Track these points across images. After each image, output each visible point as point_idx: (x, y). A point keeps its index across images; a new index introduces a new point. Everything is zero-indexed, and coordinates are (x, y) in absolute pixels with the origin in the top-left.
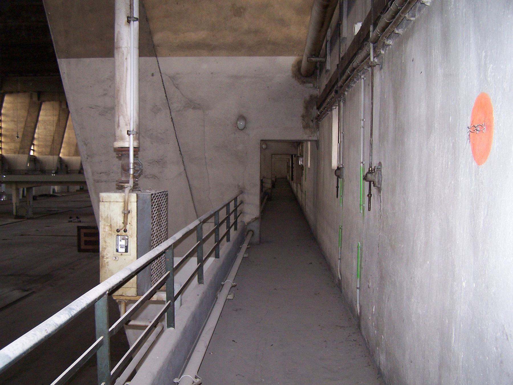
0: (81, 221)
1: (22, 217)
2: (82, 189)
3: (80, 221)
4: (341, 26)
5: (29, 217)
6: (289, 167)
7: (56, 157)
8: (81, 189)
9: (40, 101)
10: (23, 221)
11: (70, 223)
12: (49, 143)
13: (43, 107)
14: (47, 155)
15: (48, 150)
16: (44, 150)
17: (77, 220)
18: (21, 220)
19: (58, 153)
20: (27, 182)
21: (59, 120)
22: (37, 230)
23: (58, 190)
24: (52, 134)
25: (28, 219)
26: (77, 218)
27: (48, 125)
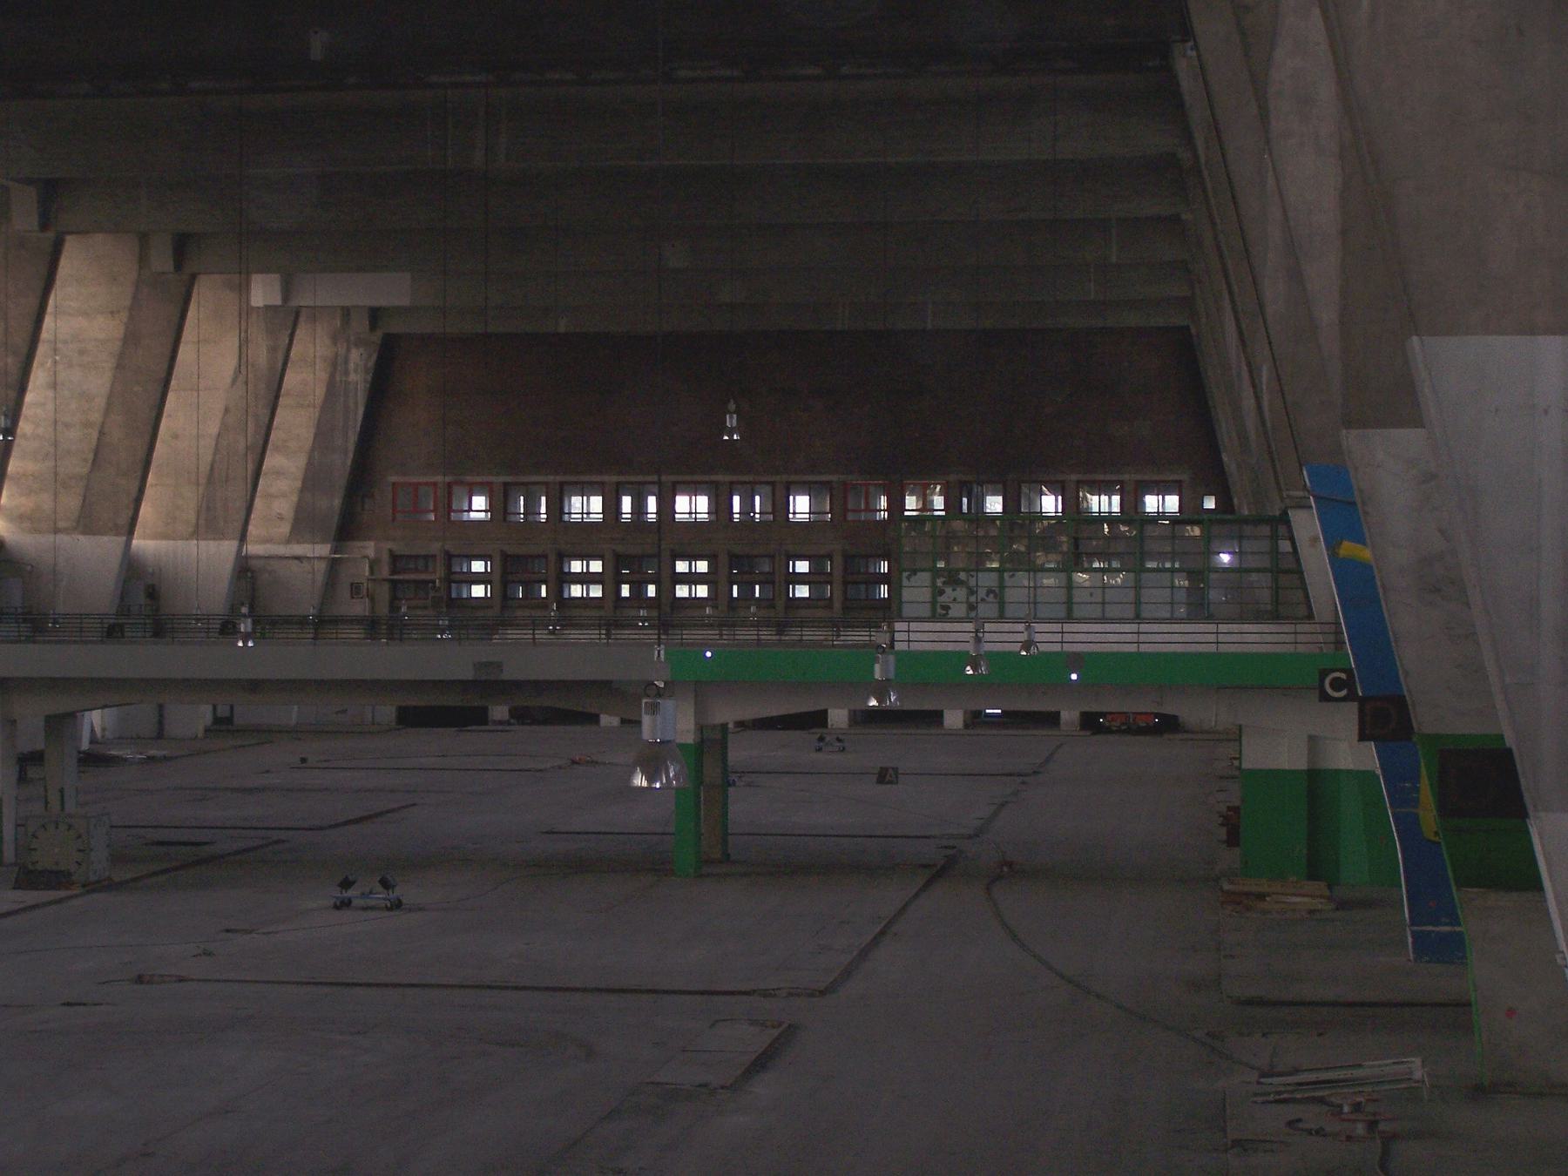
0: (404, 901)
1: (56, 879)
2: (229, 720)
3: (397, 905)
4: (1183, 66)
5: (93, 878)
6: (780, 640)
7: (228, 548)
8: (217, 720)
9: (51, 235)
10: (70, 897)
11: (346, 915)
12: (76, 466)
13: (67, 266)
14: (66, 531)
15: (71, 502)
16: (46, 501)
17: (381, 895)
18: (62, 893)
19: (123, 520)
20: (54, 684)
21: (131, 338)
22: (207, 953)
23: (104, 729)
24: (96, 417)
25: (91, 887)
26: (386, 884)
27: (70, 366)
